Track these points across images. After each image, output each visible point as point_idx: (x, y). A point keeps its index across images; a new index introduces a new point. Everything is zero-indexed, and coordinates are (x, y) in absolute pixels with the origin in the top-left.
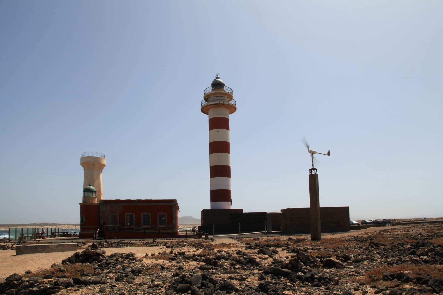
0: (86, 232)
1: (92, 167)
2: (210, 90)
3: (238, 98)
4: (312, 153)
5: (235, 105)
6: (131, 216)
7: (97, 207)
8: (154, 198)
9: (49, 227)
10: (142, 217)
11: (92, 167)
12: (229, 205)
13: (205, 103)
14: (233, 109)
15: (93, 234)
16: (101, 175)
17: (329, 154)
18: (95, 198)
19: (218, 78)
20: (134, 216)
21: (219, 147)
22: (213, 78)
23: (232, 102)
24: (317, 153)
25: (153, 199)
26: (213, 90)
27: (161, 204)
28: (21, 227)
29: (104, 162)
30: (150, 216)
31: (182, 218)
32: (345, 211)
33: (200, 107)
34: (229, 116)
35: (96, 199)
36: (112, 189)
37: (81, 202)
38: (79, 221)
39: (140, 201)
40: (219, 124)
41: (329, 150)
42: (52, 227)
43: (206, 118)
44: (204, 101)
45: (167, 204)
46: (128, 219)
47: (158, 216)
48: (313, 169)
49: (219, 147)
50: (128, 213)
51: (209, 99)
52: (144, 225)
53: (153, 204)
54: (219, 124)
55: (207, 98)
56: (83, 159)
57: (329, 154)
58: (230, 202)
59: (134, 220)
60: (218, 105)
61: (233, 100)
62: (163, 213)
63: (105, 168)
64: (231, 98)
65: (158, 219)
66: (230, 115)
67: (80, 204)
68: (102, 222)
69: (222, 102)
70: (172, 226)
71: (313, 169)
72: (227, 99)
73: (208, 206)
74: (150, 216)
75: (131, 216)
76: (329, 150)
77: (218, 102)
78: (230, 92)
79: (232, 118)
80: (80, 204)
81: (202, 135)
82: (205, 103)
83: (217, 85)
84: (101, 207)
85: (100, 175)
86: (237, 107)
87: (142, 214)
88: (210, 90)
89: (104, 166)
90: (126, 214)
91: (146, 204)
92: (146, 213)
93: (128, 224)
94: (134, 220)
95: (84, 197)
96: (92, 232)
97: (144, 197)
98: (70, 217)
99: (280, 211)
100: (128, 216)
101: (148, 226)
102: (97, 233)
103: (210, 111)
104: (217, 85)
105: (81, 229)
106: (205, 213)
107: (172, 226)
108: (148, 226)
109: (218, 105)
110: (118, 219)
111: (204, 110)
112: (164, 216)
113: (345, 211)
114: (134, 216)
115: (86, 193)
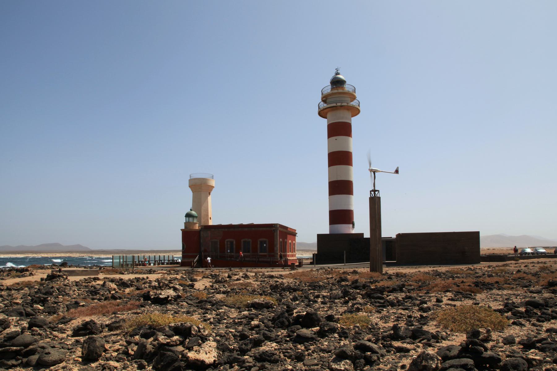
0: (186, 260)
1: (200, 188)
2: (328, 90)
3: (362, 99)
4: (375, 172)
5: (359, 106)
6: (232, 243)
7: (198, 232)
8: (256, 223)
9: (157, 255)
10: (259, 243)
11: (200, 188)
12: (349, 228)
13: (323, 105)
14: (356, 111)
15: (191, 262)
16: (210, 198)
17: (397, 172)
18: (196, 223)
19: (337, 74)
20: (234, 242)
21: (340, 158)
22: (332, 75)
23: (354, 103)
24: (379, 171)
25: (255, 223)
26: (332, 89)
27: (261, 229)
28: (143, 255)
29: (213, 183)
30: (251, 243)
31: (300, 244)
32: (474, 237)
33: (317, 110)
34: (351, 120)
35: (197, 225)
36: (223, 212)
37: (184, 228)
38: (180, 247)
39: (241, 226)
40: (339, 130)
41: (398, 168)
42: (165, 254)
43: (324, 123)
44: (322, 103)
45: (268, 229)
46: (229, 246)
47: (259, 243)
48: (374, 191)
49: (340, 158)
50: (229, 240)
51: (328, 101)
52: (261, 252)
53: (253, 229)
54: (339, 130)
55: (325, 99)
56: (190, 180)
57: (397, 172)
58: (351, 225)
59: (234, 247)
60: (338, 108)
61: (355, 101)
62: (264, 239)
63: (214, 189)
64: (354, 98)
65: (259, 246)
66: (353, 119)
67: (182, 230)
68: (203, 249)
69: (339, 104)
70: (273, 254)
71: (374, 191)
72: (349, 99)
73: (325, 230)
74: (251, 243)
75: (232, 243)
76: (398, 168)
77: (335, 105)
78: (351, 91)
79: (355, 122)
80: (182, 230)
81: (321, 146)
82: (323, 105)
83: (337, 83)
84: (202, 233)
85: (207, 198)
86: (361, 108)
87: (242, 240)
88: (328, 90)
89: (213, 187)
90: (227, 240)
91: (265, 229)
92: (246, 239)
93: (229, 251)
94: (234, 247)
95: (186, 223)
96: (190, 260)
97: (246, 222)
98: (173, 244)
99: (394, 236)
100: (229, 243)
101: (265, 254)
102: (195, 260)
103: (329, 115)
104: (337, 83)
105: (184, 257)
106: (321, 238)
107: (273, 254)
108: (265, 254)
109: (338, 108)
110: (218, 246)
111: (322, 114)
112: (265, 242)
113: (474, 237)
114: (234, 242)
115: (187, 218)
